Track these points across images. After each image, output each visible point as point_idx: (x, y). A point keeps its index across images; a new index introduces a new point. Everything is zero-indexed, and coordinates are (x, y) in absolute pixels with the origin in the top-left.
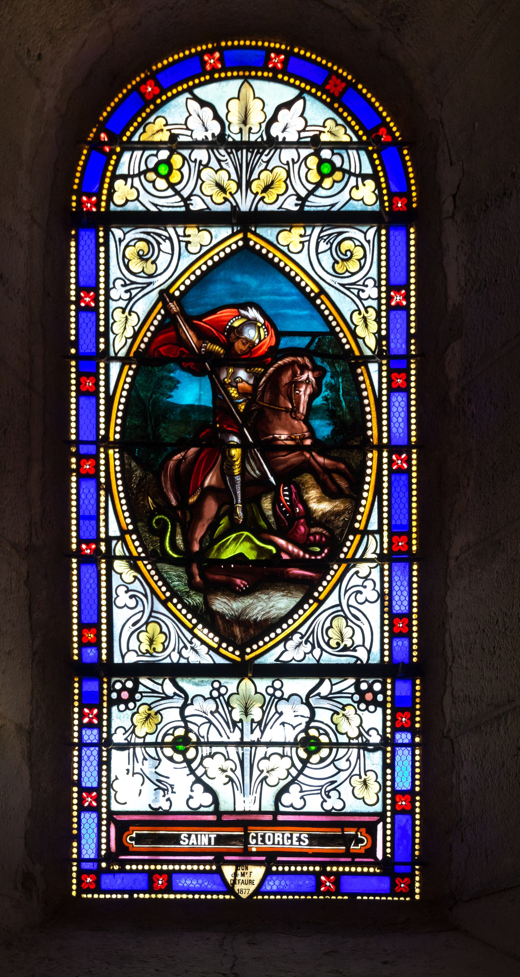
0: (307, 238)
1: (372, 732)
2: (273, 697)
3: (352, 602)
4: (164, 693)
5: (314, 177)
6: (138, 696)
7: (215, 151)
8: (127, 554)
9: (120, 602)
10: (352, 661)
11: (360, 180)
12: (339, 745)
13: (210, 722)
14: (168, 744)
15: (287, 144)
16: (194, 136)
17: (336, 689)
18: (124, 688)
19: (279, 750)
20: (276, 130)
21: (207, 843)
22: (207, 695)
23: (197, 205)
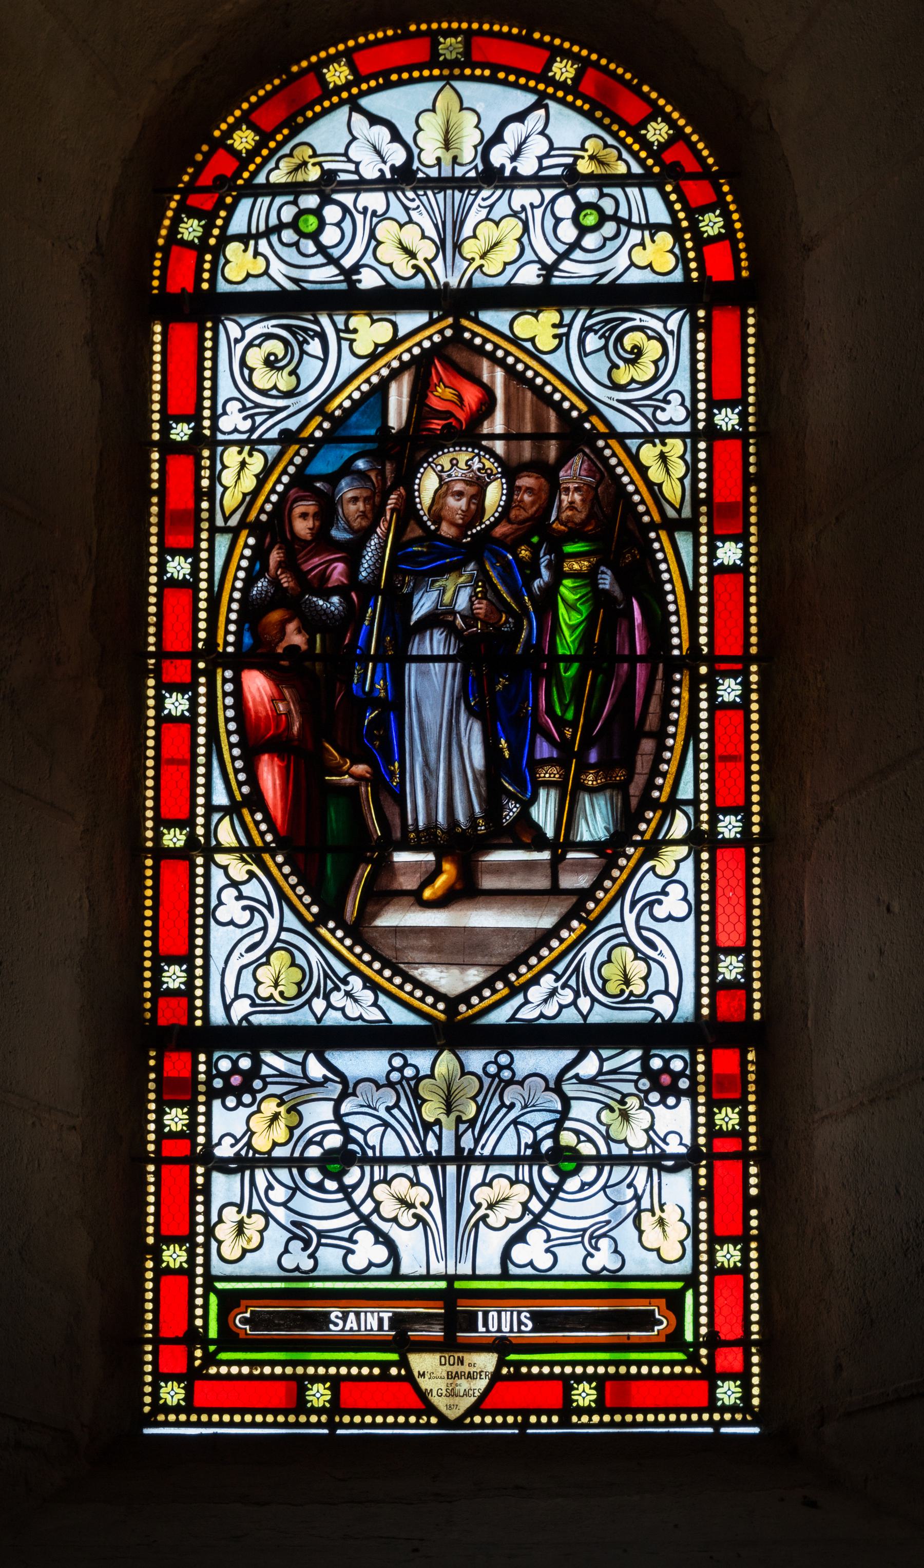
0: (564, 330)
1: (673, 1140)
2: (497, 1080)
3: (646, 920)
4: (305, 1076)
5: (568, 232)
6: (258, 1084)
7: (400, 194)
8: (245, 844)
9: (222, 914)
10: (650, 1015)
11: (647, 233)
12: (614, 1160)
13: (386, 1125)
14: (313, 1162)
15: (516, 181)
16: (362, 169)
17: (607, 1066)
18: (235, 1069)
19: (510, 1170)
20: (499, 156)
21: (375, 1327)
22: (383, 1081)
23: (368, 280)
